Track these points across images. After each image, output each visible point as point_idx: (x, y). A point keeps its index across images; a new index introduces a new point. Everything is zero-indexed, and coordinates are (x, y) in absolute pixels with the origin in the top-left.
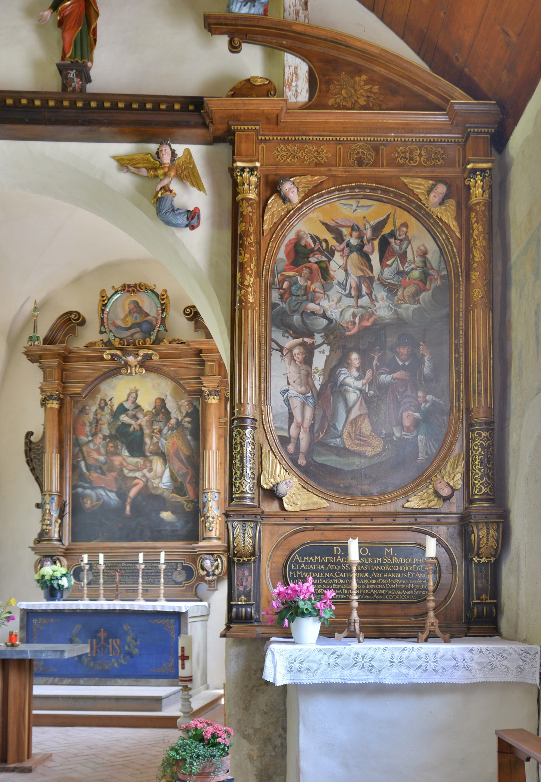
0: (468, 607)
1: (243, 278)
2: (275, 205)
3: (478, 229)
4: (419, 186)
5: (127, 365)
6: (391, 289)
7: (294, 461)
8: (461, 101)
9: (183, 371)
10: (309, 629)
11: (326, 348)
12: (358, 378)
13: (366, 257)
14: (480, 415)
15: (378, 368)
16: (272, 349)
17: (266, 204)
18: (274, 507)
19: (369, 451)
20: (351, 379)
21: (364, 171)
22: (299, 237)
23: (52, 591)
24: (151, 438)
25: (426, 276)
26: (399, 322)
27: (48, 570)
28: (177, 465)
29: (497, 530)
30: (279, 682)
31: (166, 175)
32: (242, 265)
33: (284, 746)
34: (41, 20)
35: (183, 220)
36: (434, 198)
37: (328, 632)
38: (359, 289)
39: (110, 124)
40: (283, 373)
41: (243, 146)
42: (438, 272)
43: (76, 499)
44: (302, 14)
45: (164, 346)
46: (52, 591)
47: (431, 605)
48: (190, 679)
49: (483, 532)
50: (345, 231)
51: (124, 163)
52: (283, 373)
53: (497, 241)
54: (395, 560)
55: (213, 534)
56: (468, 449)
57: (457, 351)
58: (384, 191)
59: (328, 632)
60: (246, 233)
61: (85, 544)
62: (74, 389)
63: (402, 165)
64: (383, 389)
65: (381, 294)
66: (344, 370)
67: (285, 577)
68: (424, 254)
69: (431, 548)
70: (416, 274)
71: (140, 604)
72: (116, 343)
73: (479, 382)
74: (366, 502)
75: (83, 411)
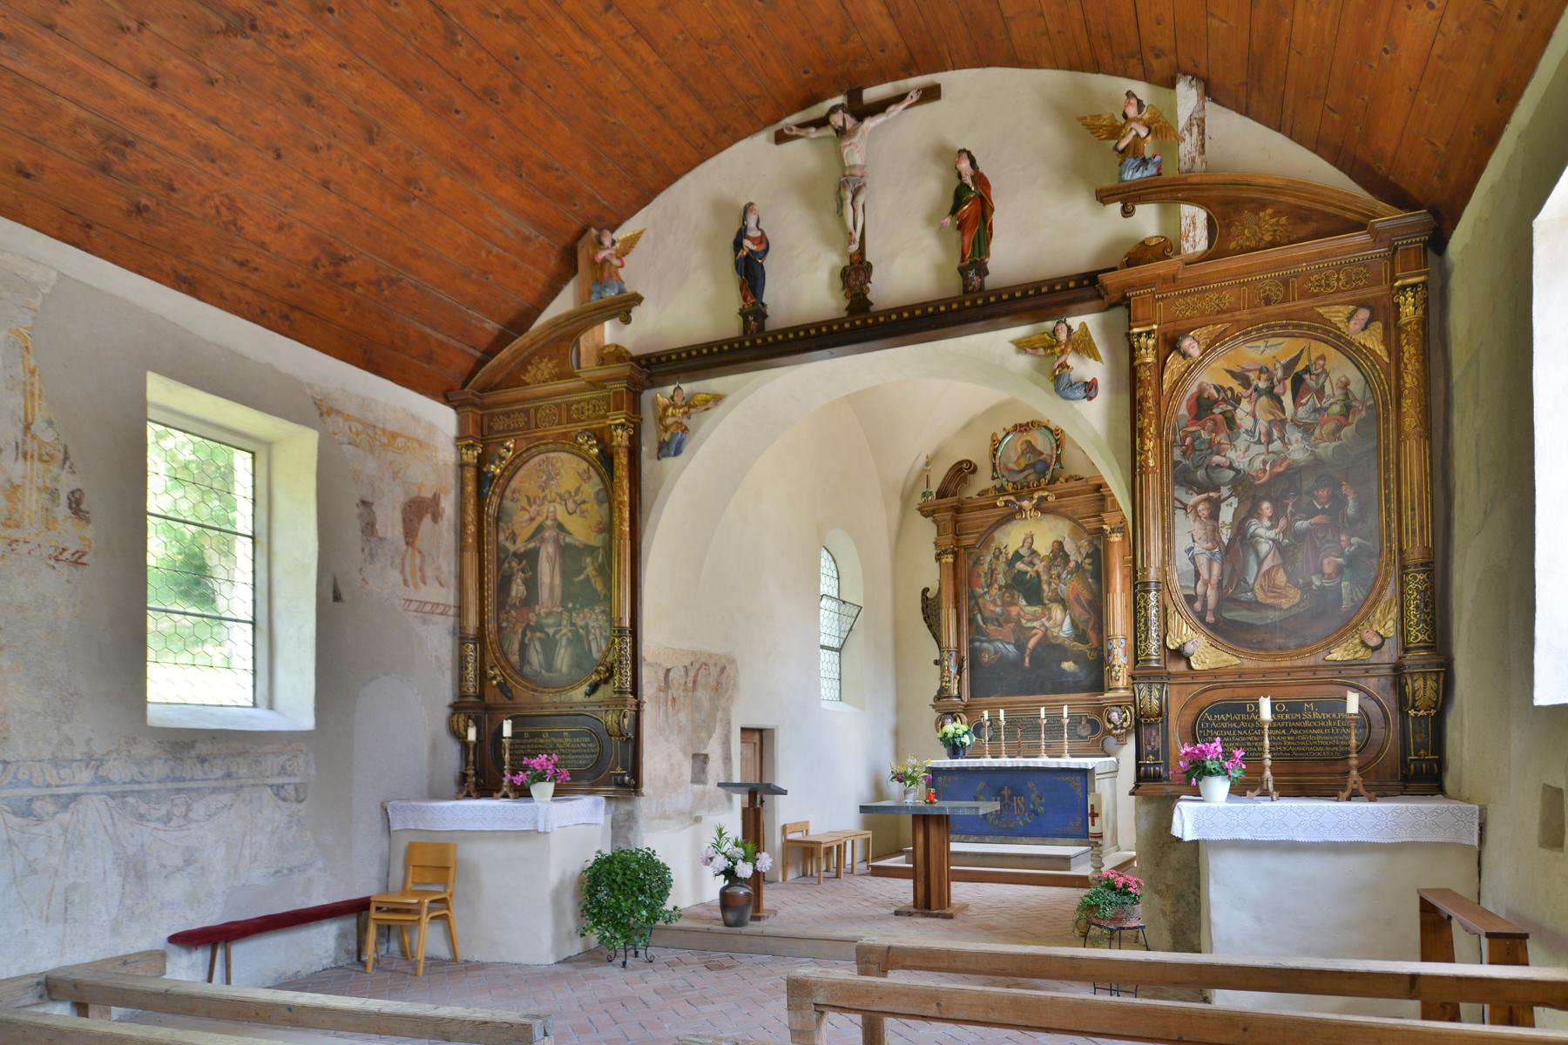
0: (1405, 763)
1: (1143, 443)
2: (1175, 363)
3: (1409, 351)
4: (1337, 314)
5: (1021, 509)
6: (1307, 429)
7: (1201, 617)
8: (1389, 217)
9: (1082, 510)
10: (1218, 788)
11: (1234, 501)
12: (1270, 528)
13: (1277, 400)
14: (1415, 555)
15: (1293, 515)
16: (1175, 508)
17: (1165, 363)
18: (1182, 666)
19: (1285, 603)
20: (1263, 530)
21: (1272, 309)
22: (1201, 390)
23: (955, 749)
24: (1050, 584)
25: (1348, 408)
26: (1317, 463)
27: (950, 728)
28: (1078, 611)
29: (1437, 681)
30: (1187, 838)
31: (1063, 352)
32: (1141, 430)
33: (1198, 902)
34: (942, 227)
35: (1080, 393)
36: (1355, 325)
37: (1238, 790)
38: (1269, 434)
39: (1007, 314)
40: (1188, 532)
41: (1139, 312)
42: (1363, 403)
43: (974, 654)
44: (1198, 160)
45: (1060, 486)
46: (955, 749)
47: (1354, 762)
48: (1100, 836)
49: (1419, 683)
50: (1252, 375)
51: (1022, 346)
52: (1188, 532)
53: (1436, 357)
54: (1316, 715)
55: (1120, 684)
56: (1402, 593)
57: (1387, 487)
58: (1295, 326)
59: (1238, 790)
60: (1145, 398)
61: (984, 700)
62: (968, 540)
63: (1316, 295)
64: (1299, 536)
65: (1294, 436)
66: (1254, 521)
67: (1194, 735)
68: (1345, 386)
69: (1353, 703)
70: (1336, 409)
71: (1044, 761)
72: (1010, 488)
73: (1412, 520)
74: (1282, 657)
75: (977, 562)
